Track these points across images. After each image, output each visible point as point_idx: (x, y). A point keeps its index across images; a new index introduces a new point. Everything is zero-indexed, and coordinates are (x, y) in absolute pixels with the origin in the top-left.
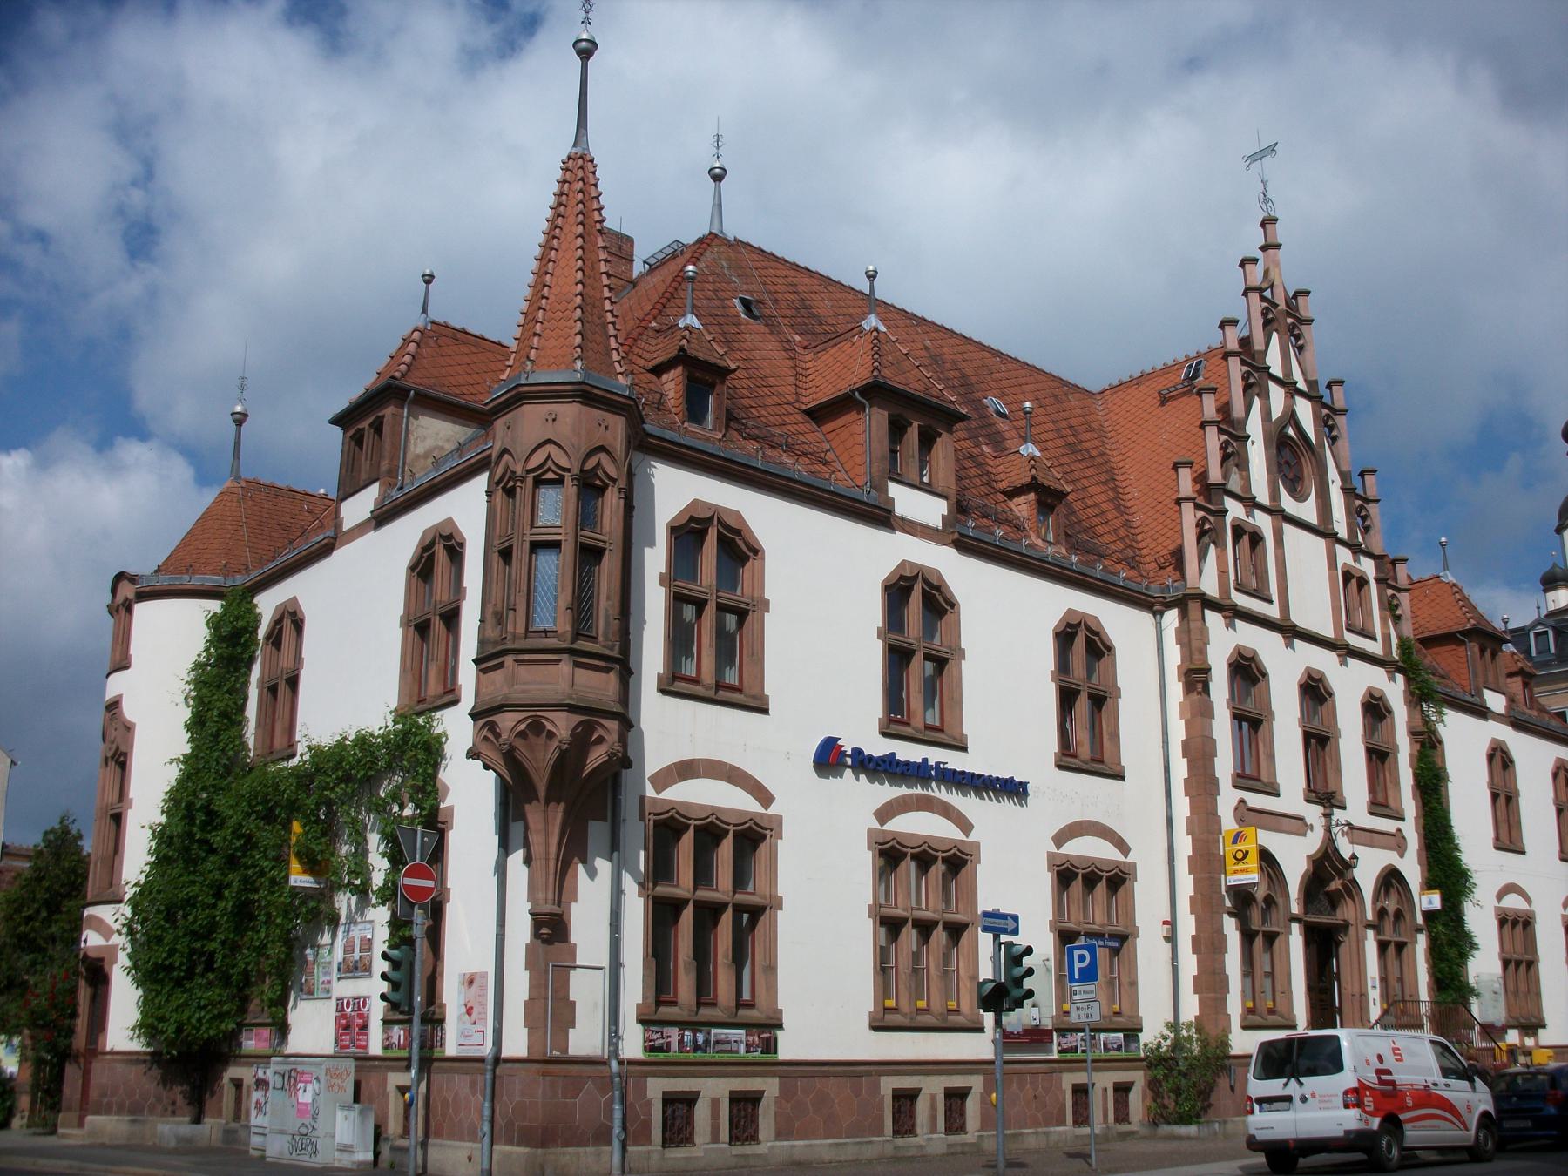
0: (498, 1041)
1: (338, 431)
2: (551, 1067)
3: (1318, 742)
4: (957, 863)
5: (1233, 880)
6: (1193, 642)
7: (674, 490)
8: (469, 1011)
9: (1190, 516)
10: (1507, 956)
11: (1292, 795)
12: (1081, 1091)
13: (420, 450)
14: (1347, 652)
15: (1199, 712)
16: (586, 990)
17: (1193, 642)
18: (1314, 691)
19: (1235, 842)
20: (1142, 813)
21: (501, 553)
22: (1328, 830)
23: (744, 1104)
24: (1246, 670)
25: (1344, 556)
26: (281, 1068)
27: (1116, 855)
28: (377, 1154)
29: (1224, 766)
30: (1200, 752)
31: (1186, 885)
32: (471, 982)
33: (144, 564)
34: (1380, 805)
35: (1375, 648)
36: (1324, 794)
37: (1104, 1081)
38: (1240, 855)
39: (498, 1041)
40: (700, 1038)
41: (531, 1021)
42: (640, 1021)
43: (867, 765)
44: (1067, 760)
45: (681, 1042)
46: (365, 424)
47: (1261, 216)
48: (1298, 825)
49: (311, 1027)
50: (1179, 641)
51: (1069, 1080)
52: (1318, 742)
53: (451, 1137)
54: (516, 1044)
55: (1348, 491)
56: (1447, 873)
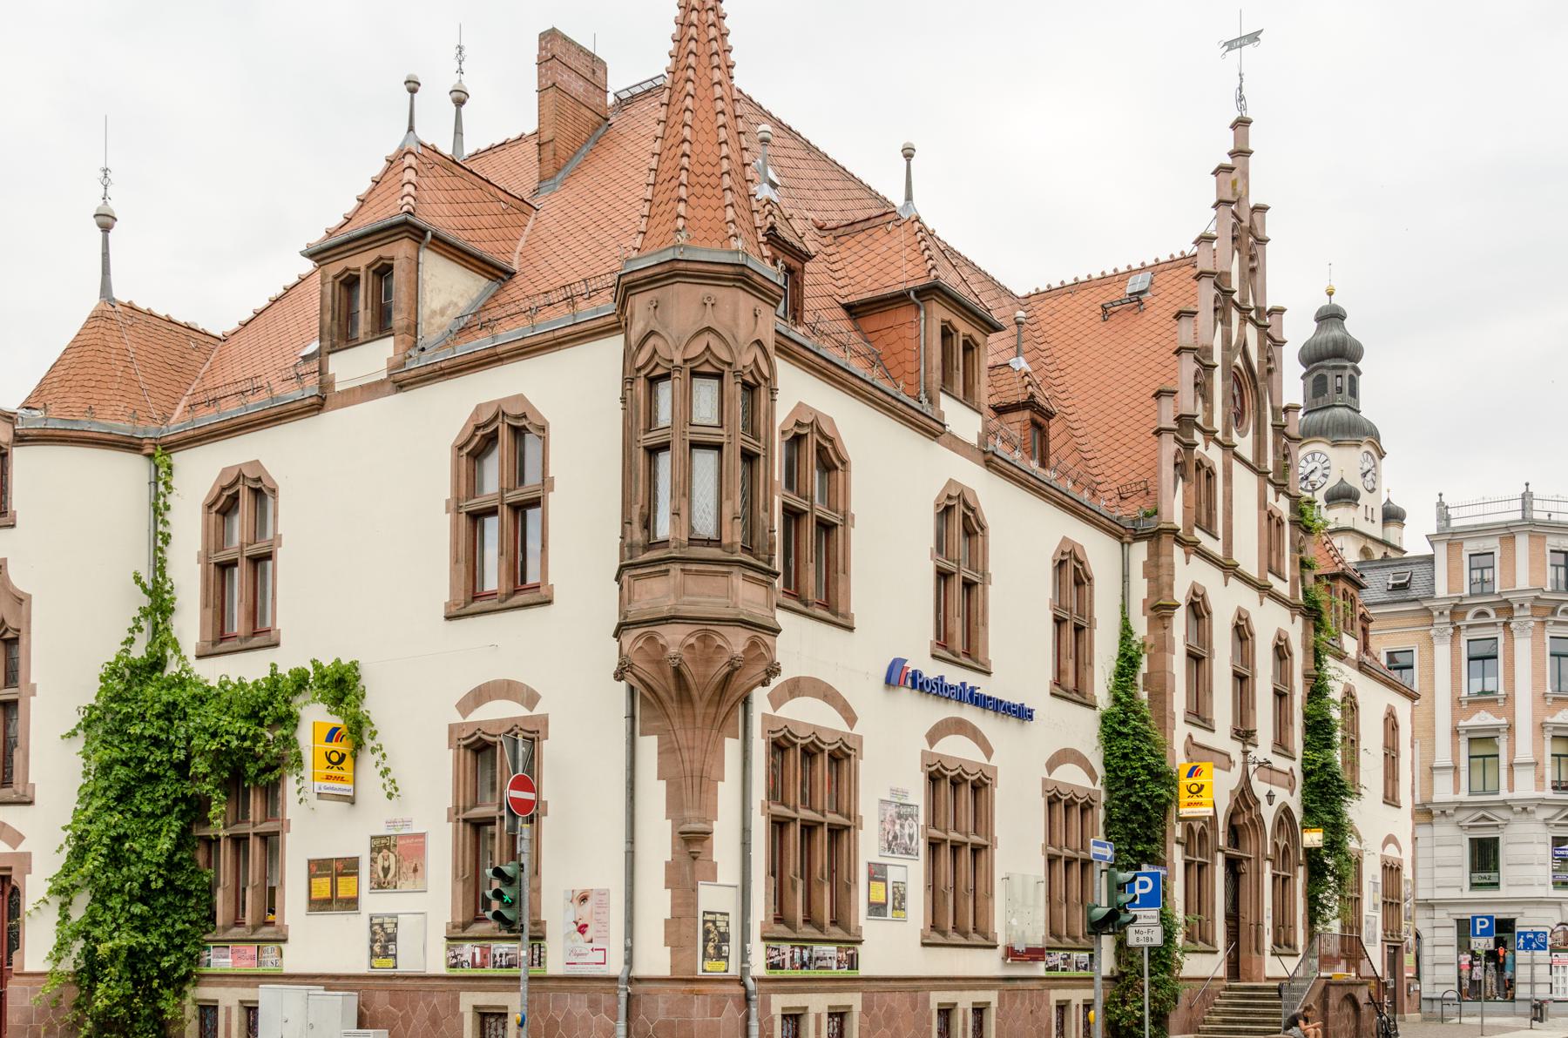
0: (629, 961)
2: (696, 987)
5: (1185, 812)
6: (1157, 572)
8: (582, 929)
9: (1169, 447)
10: (1053, 850)
11: (1222, 738)
12: (1062, 1007)
14: (1264, 589)
17: (1157, 572)
18: (1242, 632)
19: (1190, 775)
21: (645, 450)
22: (1245, 763)
24: (1198, 609)
25: (1270, 490)
27: (839, 724)
32: (584, 899)
35: (1283, 588)
36: (1244, 734)
37: (818, 1004)
38: (1194, 789)
39: (629, 961)
40: (806, 954)
42: (764, 939)
43: (918, 683)
45: (792, 958)
46: (360, 262)
47: (1235, 115)
50: (1146, 575)
51: (1056, 995)
54: (655, 960)
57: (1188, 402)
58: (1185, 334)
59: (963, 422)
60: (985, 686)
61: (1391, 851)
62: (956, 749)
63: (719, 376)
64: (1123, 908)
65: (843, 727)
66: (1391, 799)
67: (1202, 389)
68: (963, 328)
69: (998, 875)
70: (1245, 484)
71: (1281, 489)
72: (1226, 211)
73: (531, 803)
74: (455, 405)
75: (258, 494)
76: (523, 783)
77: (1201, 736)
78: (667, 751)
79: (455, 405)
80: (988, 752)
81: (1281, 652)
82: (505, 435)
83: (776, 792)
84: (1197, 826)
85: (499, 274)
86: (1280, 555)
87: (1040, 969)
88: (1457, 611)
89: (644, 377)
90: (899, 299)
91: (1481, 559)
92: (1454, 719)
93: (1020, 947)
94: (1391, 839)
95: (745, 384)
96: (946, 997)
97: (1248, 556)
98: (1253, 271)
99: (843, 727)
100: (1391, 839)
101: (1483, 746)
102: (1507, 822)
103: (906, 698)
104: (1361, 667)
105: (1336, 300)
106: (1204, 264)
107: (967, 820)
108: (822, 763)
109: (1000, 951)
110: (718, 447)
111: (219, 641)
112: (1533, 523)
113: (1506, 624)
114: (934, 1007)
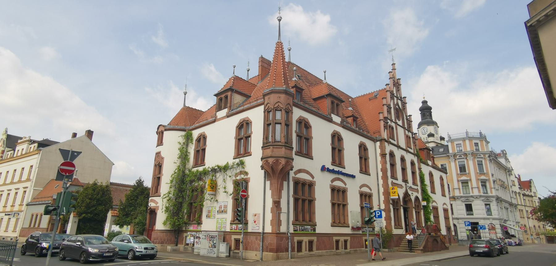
0: (263, 229)
1: (215, 98)
3: (404, 170)
4: (344, 192)
5: (392, 197)
6: (382, 148)
7: (297, 113)
8: (255, 222)
9: (382, 123)
11: (400, 181)
13: (235, 102)
15: (384, 163)
16: (283, 217)
18: (403, 159)
20: (374, 182)
21: (267, 125)
23: (311, 243)
24: (392, 155)
25: (407, 132)
26: (205, 234)
28: (229, 253)
29: (389, 174)
30: (384, 171)
31: (382, 198)
33: (166, 124)
34: (414, 183)
35: (412, 151)
36: (405, 181)
37: (306, 239)
39: (263, 229)
41: (272, 224)
44: (361, 171)
46: (223, 96)
48: (401, 186)
49: (209, 224)
52: (404, 170)
53: (250, 250)
54: (269, 229)
55: (407, 119)
56: (426, 198)
57: (386, 115)
58: (384, 101)
59: (337, 119)
60: (344, 171)
61: (445, 206)
62: (338, 184)
63: (281, 110)
64: (372, 218)
65: (311, 179)
66: (444, 195)
67: (389, 112)
68: (336, 102)
69: (349, 211)
70: (401, 131)
71: (409, 131)
72: (392, 80)
73: (245, 195)
74: (236, 119)
75: (204, 137)
76: (243, 191)
77: (395, 181)
78: (271, 184)
79: (236, 119)
80: (345, 184)
81: (412, 164)
82: (245, 124)
83: (295, 192)
84: (396, 201)
85: (248, 97)
86: (410, 144)
87: (361, 232)
88: (455, 155)
89: (267, 112)
90: (322, 97)
91: (459, 145)
92: (457, 178)
93: (355, 227)
94: (444, 204)
95: (286, 111)
96: (338, 238)
97: (403, 144)
98: (398, 90)
99: (311, 179)
100: (444, 204)
101: (465, 183)
102: (473, 201)
103: (326, 174)
104: (433, 167)
105: (425, 99)
106: (388, 89)
107: (341, 199)
108: (307, 187)
109: (350, 227)
110: (280, 123)
111: (196, 165)
112: (469, 137)
113: (466, 158)
114: (334, 240)
